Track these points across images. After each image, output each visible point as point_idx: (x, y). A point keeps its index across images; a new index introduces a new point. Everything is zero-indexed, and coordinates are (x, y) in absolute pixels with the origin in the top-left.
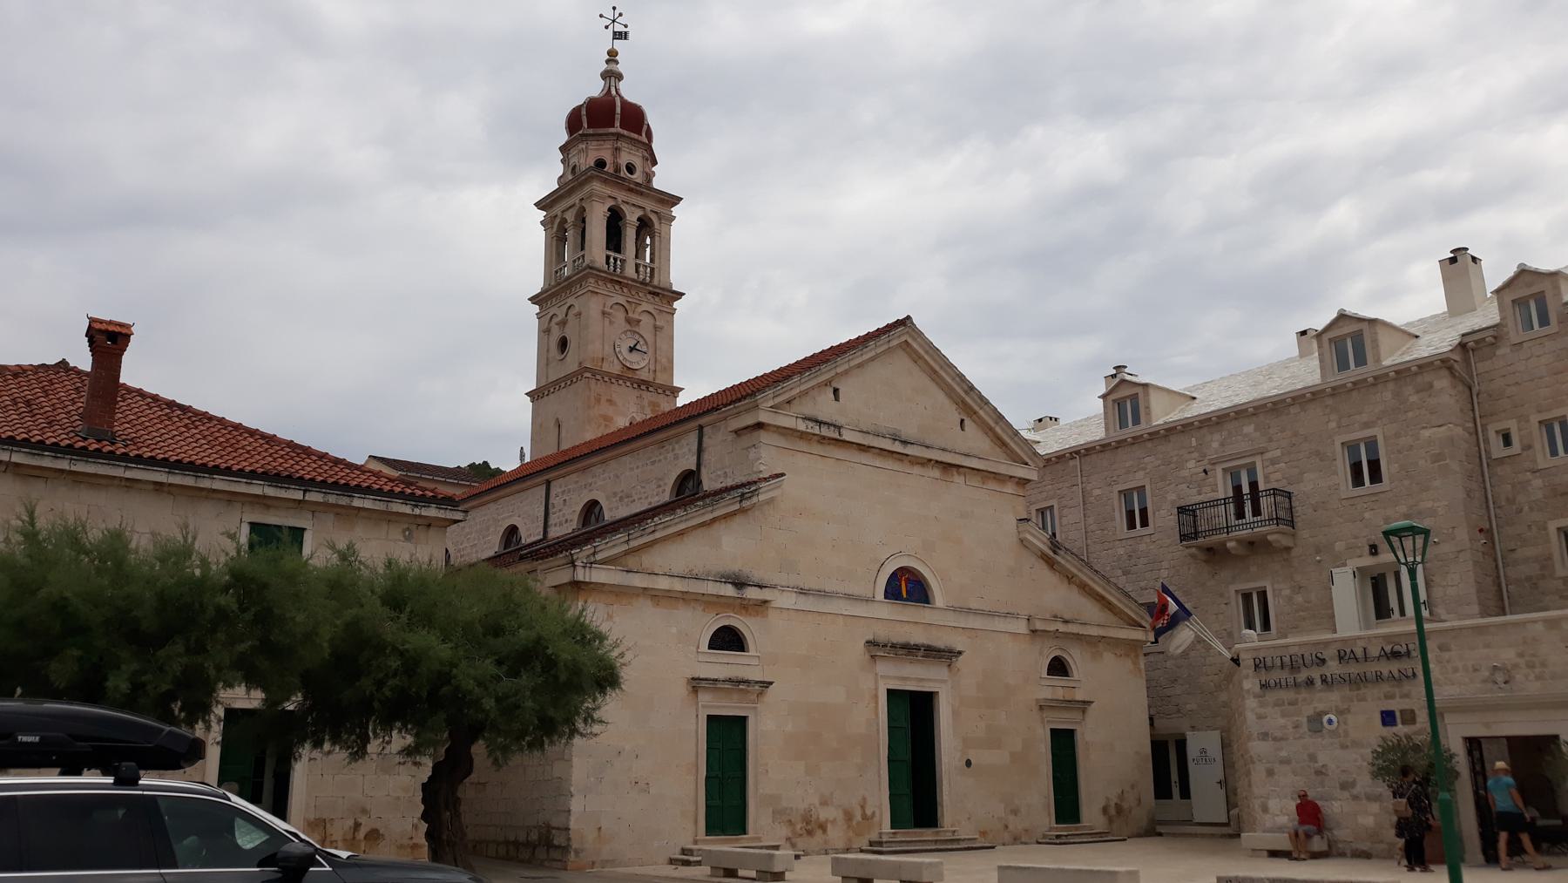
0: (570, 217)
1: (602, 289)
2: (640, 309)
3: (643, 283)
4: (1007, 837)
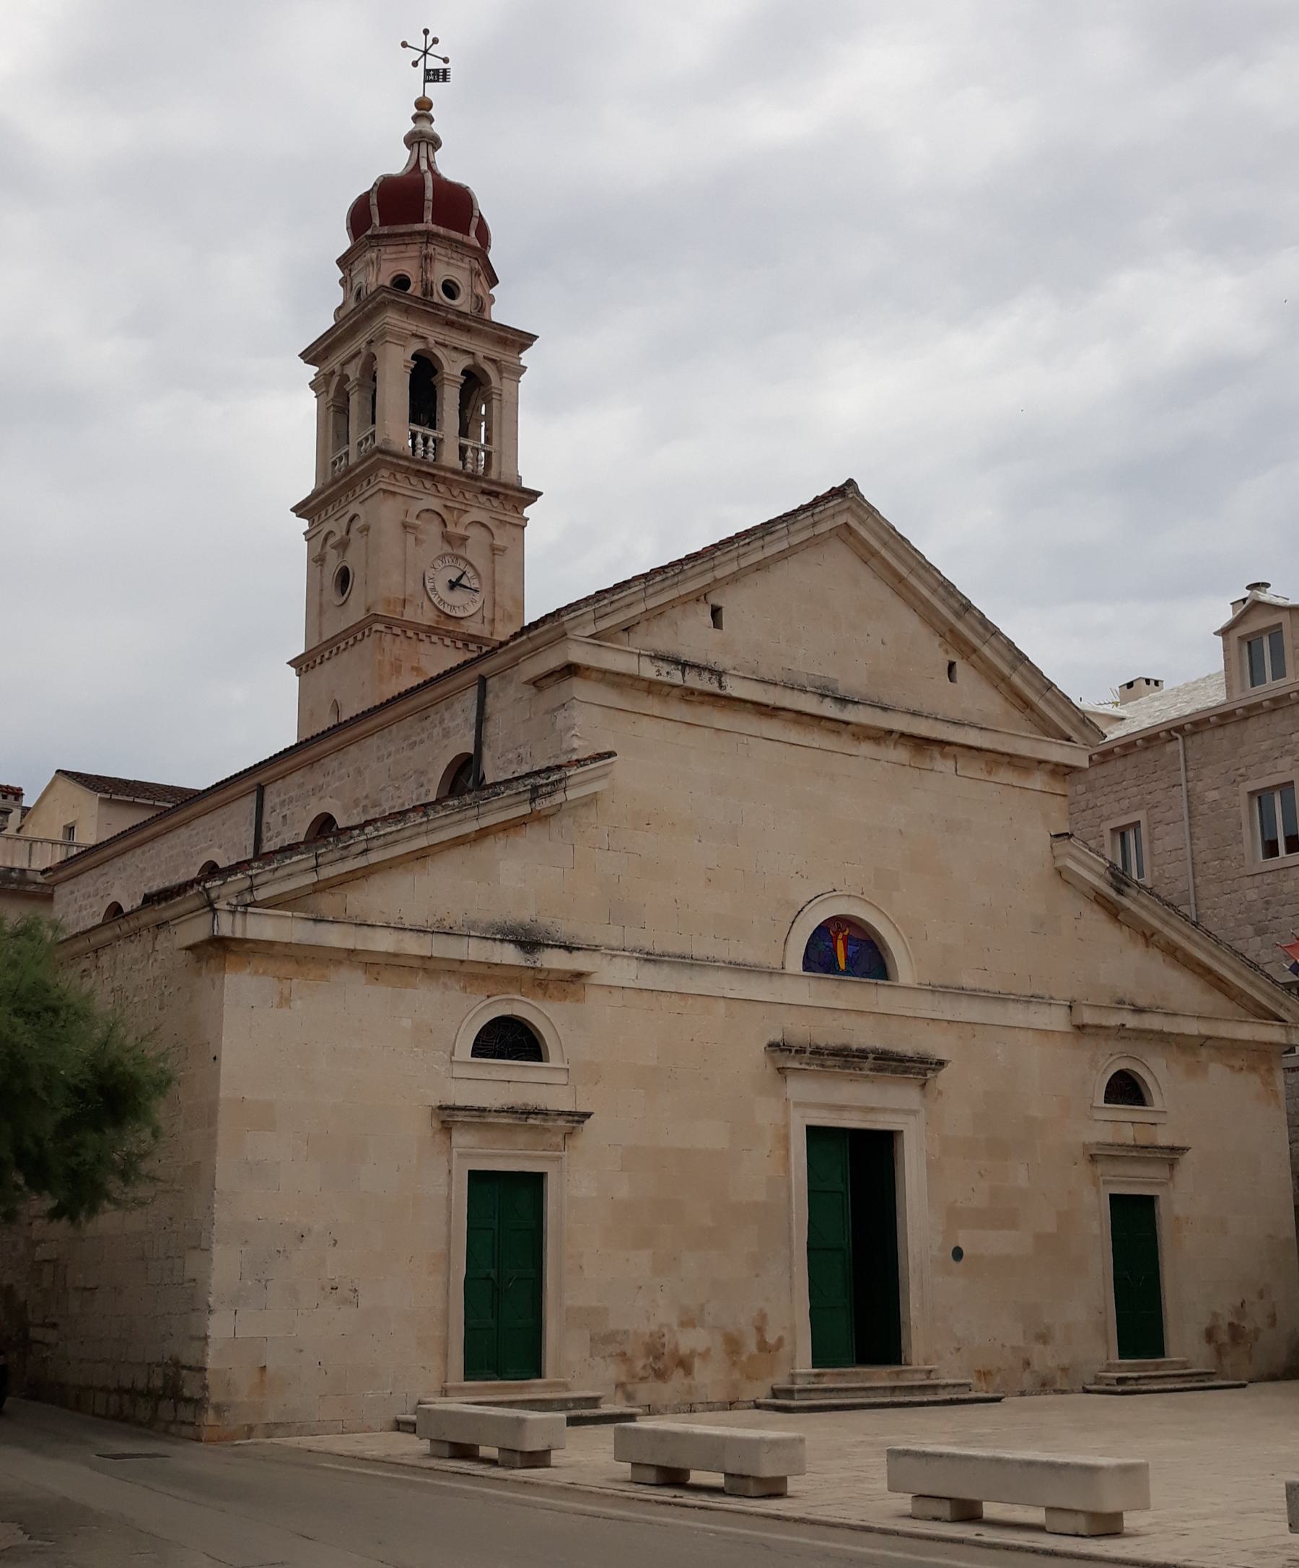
0: (353, 371)
1: (403, 485)
2: (467, 519)
3: (473, 477)
4: (1027, 1380)
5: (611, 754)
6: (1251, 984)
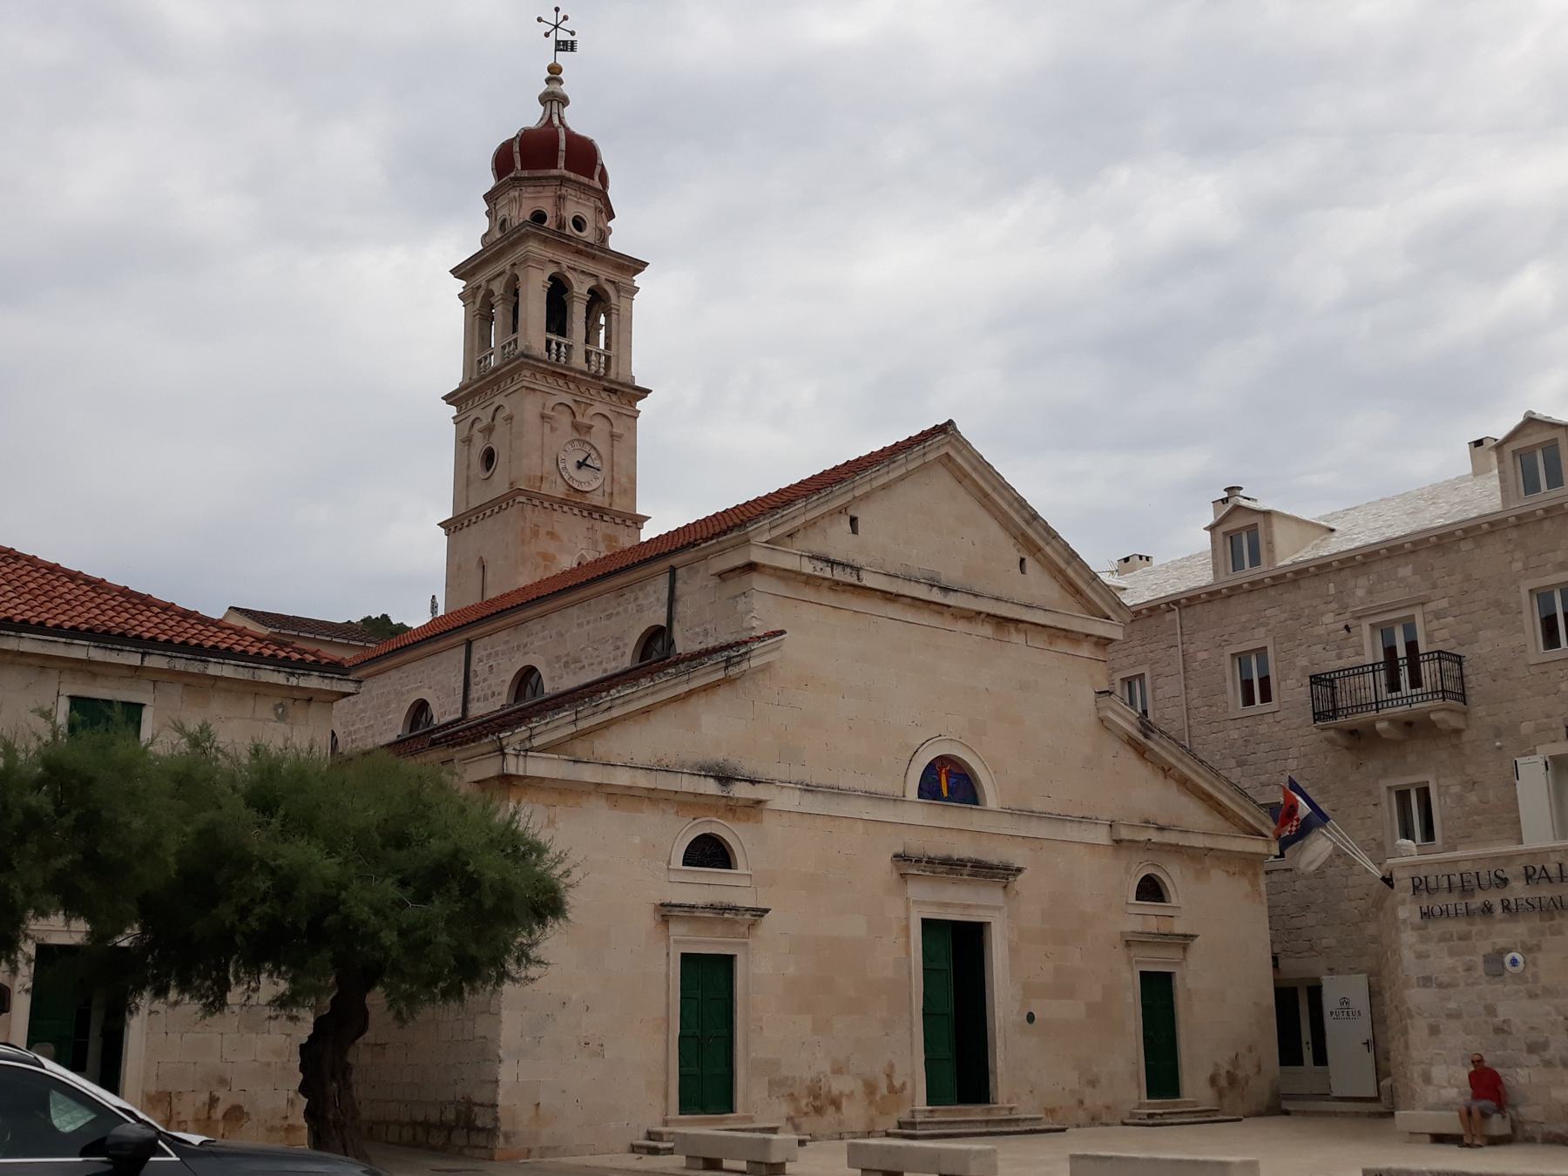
0: (498, 287)
1: (540, 384)
2: (591, 411)
3: (596, 376)
4: (1082, 1116)
5: (782, 632)
6: (1242, 807)
